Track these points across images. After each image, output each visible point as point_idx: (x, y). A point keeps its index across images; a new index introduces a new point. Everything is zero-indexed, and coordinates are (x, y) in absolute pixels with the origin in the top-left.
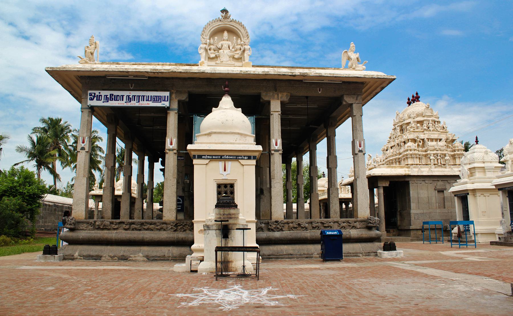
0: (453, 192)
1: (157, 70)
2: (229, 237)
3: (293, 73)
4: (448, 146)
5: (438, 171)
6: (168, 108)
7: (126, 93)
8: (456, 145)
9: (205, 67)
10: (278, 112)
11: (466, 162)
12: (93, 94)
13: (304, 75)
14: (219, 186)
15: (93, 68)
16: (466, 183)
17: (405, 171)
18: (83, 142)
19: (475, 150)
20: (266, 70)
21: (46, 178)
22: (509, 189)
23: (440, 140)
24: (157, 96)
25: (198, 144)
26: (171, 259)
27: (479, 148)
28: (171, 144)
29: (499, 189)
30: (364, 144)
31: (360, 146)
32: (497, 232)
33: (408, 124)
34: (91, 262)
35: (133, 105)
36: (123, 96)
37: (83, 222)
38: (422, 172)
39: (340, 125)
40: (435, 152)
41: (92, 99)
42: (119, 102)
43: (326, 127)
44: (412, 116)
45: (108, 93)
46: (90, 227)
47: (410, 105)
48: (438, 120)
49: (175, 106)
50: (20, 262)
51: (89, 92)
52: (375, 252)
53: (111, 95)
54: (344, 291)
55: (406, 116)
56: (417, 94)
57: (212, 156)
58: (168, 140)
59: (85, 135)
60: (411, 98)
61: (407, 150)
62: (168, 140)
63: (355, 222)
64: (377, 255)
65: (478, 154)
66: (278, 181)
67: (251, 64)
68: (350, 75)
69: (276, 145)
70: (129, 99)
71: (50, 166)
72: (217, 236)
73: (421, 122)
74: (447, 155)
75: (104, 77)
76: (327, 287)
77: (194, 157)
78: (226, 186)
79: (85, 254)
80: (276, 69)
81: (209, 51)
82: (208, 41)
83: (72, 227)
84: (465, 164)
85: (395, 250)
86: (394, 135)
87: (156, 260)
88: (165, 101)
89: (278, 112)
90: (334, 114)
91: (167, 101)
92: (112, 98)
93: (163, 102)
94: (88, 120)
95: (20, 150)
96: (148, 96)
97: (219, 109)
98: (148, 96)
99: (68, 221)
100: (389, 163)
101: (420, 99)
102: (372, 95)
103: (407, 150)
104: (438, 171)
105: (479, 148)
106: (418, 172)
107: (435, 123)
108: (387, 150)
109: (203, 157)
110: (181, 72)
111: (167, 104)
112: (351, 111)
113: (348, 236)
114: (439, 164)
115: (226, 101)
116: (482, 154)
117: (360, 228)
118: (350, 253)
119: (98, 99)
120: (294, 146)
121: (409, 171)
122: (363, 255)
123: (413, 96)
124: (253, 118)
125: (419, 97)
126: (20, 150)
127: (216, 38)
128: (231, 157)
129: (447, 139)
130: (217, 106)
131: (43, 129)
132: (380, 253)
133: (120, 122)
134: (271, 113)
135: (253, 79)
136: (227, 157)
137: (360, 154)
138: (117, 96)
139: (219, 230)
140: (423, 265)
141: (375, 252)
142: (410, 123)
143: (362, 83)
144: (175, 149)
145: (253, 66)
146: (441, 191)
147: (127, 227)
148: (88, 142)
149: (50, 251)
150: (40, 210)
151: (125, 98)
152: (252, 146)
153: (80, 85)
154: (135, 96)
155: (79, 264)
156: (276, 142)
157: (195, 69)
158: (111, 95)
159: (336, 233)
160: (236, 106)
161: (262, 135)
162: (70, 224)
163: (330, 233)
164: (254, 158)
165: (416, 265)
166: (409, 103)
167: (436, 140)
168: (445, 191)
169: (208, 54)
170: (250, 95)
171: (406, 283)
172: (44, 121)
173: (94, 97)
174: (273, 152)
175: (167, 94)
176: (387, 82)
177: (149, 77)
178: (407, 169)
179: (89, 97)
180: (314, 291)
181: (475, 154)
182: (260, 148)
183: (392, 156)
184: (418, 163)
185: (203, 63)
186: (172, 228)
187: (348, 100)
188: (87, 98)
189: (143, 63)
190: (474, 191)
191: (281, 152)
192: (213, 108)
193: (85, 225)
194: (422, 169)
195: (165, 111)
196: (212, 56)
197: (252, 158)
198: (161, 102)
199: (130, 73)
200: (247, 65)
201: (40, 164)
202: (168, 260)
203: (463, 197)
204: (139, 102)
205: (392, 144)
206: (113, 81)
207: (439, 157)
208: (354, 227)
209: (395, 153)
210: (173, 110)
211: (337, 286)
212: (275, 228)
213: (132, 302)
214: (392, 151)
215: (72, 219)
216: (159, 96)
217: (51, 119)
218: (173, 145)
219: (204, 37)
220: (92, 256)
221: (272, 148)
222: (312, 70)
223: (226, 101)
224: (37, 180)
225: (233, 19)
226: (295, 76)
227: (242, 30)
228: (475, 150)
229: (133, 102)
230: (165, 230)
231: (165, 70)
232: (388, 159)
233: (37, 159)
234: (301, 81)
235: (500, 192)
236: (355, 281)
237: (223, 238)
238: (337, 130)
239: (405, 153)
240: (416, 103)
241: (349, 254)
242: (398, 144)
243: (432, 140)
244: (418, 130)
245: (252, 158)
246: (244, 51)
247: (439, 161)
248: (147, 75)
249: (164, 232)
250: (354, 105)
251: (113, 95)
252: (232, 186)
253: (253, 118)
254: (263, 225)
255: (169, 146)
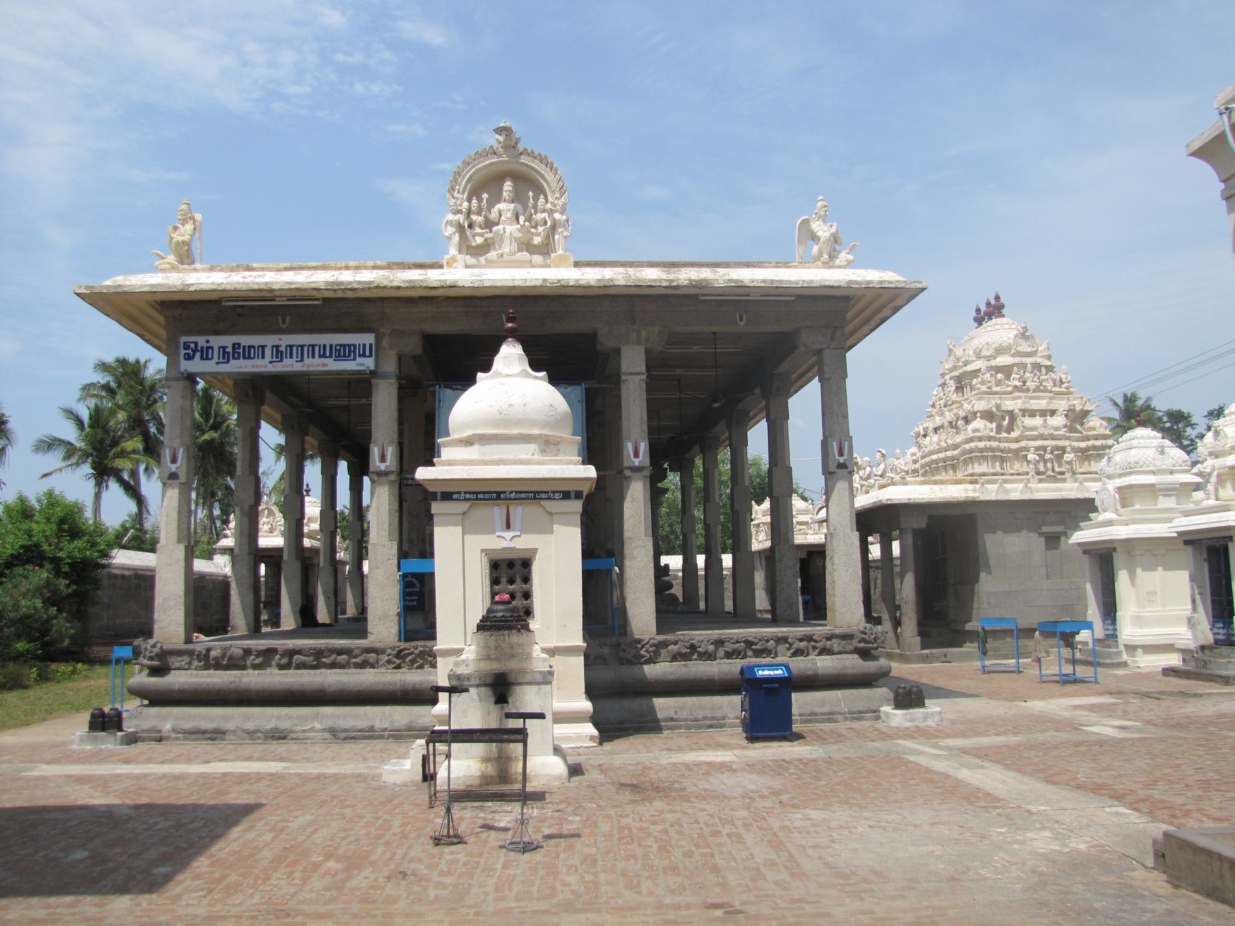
0: (1079, 544)
1: (342, 283)
2: (510, 700)
3: (671, 281)
4: (1072, 429)
5: (1047, 490)
6: (373, 374)
7: (269, 340)
8: (1091, 424)
9: (461, 273)
10: (638, 374)
11: (1110, 470)
12: (192, 345)
13: (700, 285)
14: (495, 565)
15: (188, 285)
16: (1110, 523)
17: (966, 490)
18: (174, 461)
19: (1134, 442)
20: (607, 274)
21: (115, 509)
22: (1210, 543)
23: (1053, 413)
24: (344, 346)
25: (452, 464)
26: (389, 736)
27: (1143, 438)
28: (383, 459)
29: (1187, 543)
30: (851, 447)
31: (841, 454)
32: (1181, 644)
33: (975, 373)
34: (204, 746)
35: (289, 369)
36: (263, 347)
37: (179, 653)
38: (1007, 492)
39: (802, 387)
40: (1039, 443)
41: (189, 357)
42: (256, 362)
43: (766, 395)
44: (985, 353)
45: (228, 341)
46: (195, 663)
47: (980, 324)
48: (1048, 363)
49: (390, 366)
50: (34, 754)
51: (184, 339)
52: (874, 712)
53: (236, 346)
54: (762, 853)
55: (971, 352)
56: (997, 298)
57: (477, 493)
58: (376, 449)
59: (177, 443)
60: (983, 308)
61: (971, 440)
62: (376, 449)
63: (828, 639)
64: (878, 718)
65: (1142, 451)
66: (641, 543)
67: (572, 260)
68: (812, 281)
69: (636, 455)
70: (279, 354)
71: (126, 477)
72: (481, 700)
73: (1007, 371)
74: (1068, 449)
75: (217, 302)
76: (724, 839)
77: (434, 497)
78: (511, 564)
79: (188, 725)
80: (631, 271)
81: (468, 232)
82: (466, 204)
83: (156, 663)
84: (1109, 477)
85: (922, 705)
86: (941, 399)
87: (353, 738)
88: (364, 355)
89: (638, 374)
90: (784, 367)
91: (371, 355)
92: (239, 352)
93: (360, 360)
94: (182, 408)
95: (48, 445)
96: (325, 346)
97: (492, 377)
98: (325, 346)
99: (146, 649)
100: (930, 470)
101: (1004, 311)
102: (873, 323)
103: (971, 440)
104: (1047, 490)
105: (1143, 438)
106: (997, 492)
107: (1040, 371)
108: (925, 436)
109: (455, 496)
110: (398, 288)
111: (369, 363)
112: (820, 363)
113: (810, 673)
114: (1050, 473)
115: (510, 356)
116: (1151, 453)
117: (840, 653)
118: (816, 714)
119: (205, 357)
120: (670, 450)
121: (975, 490)
122: (846, 719)
123: (988, 304)
124: (578, 391)
125: (1003, 306)
126: (48, 445)
127: (485, 196)
128: (523, 495)
129: (1069, 410)
130: (487, 367)
131: (106, 387)
132: (887, 714)
133: (269, 395)
134: (623, 377)
135: (576, 297)
136: (513, 495)
137: (841, 471)
138: (250, 347)
139: (485, 685)
140: (983, 754)
141: (874, 712)
142: (979, 370)
143: (846, 299)
144: (391, 472)
145: (577, 264)
146: (1053, 541)
147: (285, 661)
148: (185, 460)
149: (105, 722)
150: (104, 595)
151: (268, 351)
152: (572, 467)
153: (161, 319)
154: (291, 347)
155: (170, 756)
156: (636, 449)
157: (434, 277)
158: (236, 346)
159: (780, 672)
160: (535, 365)
161: (598, 441)
162: (151, 658)
163: (766, 673)
164: (578, 495)
165: (965, 751)
166: (979, 321)
167: (1043, 413)
168: (1063, 538)
169: (467, 239)
170: (565, 337)
171: (916, 826)
172: (103, 367)
173: (195, 351)
174: (627, 473)
175: (368, 339)
176: (906, 297)
177: (324, 299)
178: (970, 487)
179: (183, 352)
180: (689, 854)
181: (1133, 452)
182: (591, 472)
183: (938, 451)
184: (998, 469)
185: (453, 260)
186: (389, 662)
187: (809, 340)
188: (178, 355)
189: (309, 264)
190: (1129, 543)
191: (647, 473)
192: (480, 375)
193: (186, 659)
194: (1007, 486)
195: (361, 385)
196: (479, 240)
197: (573, 495)
198: (355, 359)
199: (277, 294)
200: (559, 263)
201: (103, 472)
202: (382, 737)
203: (1104, 560)
204: (302, 360)
205: (938, 421)
206: (239, 310)
207: (1048, 456)
208: (825, 651)
209: (943, 444)
210: (385, 376)
211: (749, 838)
212: (635, 656)
213: (257, 899)
214: (935, 438)
215: (154, 646)
216: (349, 346)
217: (123, 362)
218: (388, 463)
219: (456, 194)
220: (204, 732)
221: (626, 464)
222: (721, 271)
223: (510, 356)
224: (91, 522)
225: (526, 150)
226: (677, 287)
227: (549, 176)
228: (1134, 442)
229: (287, 361)
230: (373, 666)
231: (359, 282)
232: (928, 459)
233: (94, 462)
234: (696, 296)
235: (1190, 548)
236: (796, 818)
237: (496, 703)
238: (790, 401)
239: (967, 446)
240: (994, 321)
241: (811, 717)
242: (950, 423)
243: (1032, 413)
244: (998, 389)
245: (573, 495)
246: (554, 228)
247: (1049, 465)
248: (317, 295)
249: (372, 670)
250: (826, 353)
251: (239, 344)
252: (526, 564)
253: (578, 391)
254: (606, 650)
255: (378, 463)
